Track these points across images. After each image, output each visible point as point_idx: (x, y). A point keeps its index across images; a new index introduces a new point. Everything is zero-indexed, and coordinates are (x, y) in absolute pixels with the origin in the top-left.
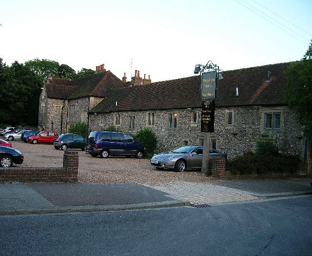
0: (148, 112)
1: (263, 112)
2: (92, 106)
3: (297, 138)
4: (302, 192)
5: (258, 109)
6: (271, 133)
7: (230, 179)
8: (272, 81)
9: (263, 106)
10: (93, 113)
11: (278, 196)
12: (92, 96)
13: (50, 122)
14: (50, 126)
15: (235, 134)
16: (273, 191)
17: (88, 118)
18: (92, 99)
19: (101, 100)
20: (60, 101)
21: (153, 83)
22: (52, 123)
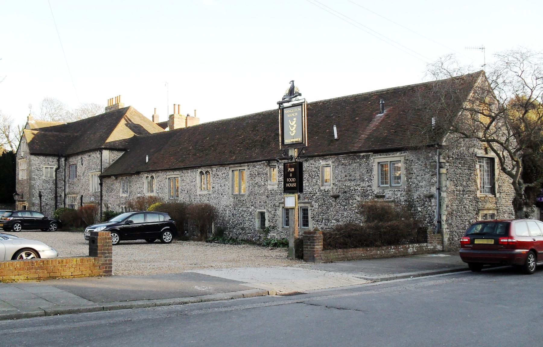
0: (200, 170)
1: (376, 160)
2: (106, 165)
3: (426, 196)
4: (421, 272)
5: (368, 157)
6: (387, 191)
7: (252, 294)
8: (387, 115)
9: (376, 152)
10: (109, 176)
11: (390, 279)
12: (105, 149)
13: (37, 194)
14: (37, 202)
15: (336, 197)
16: (387, 272)
17: (101, 184)
18: (106, 153)
19: (121, 154)
20: (50, 159)
21: (177, 129)
22: (40, 196)
